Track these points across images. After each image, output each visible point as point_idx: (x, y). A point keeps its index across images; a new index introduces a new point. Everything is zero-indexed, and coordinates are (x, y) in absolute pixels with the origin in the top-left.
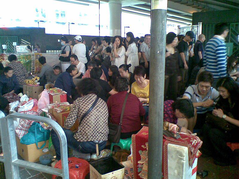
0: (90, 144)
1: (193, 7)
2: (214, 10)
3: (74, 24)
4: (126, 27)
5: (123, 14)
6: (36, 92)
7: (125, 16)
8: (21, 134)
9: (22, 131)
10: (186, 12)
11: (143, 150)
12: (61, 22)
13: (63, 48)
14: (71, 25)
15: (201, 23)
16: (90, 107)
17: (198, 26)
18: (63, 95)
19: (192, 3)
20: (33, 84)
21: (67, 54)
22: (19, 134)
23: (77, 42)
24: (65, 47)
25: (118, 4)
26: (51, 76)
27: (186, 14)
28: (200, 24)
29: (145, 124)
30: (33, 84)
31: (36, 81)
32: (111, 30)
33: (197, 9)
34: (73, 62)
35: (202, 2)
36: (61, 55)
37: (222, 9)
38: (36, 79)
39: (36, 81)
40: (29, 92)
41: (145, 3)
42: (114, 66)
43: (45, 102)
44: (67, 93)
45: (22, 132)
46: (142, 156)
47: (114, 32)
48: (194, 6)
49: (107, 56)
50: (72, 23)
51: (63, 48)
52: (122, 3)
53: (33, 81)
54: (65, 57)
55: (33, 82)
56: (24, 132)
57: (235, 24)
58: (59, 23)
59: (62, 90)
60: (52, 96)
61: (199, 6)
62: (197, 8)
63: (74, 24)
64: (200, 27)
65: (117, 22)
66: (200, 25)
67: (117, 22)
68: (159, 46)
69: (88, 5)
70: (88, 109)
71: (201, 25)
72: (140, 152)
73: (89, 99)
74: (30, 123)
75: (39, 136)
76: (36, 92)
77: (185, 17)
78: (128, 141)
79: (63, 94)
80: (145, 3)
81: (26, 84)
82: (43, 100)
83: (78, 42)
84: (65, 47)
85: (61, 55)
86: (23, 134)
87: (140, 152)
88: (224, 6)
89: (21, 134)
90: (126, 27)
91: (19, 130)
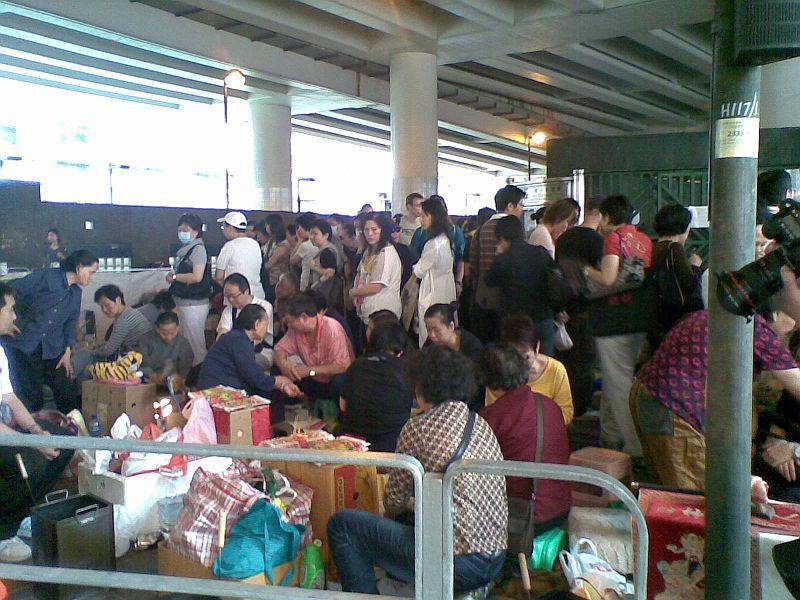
0: (472, 561)
1: (511, 120)
2: (584, 134)
3: (20, 159)
4: (304, 179)
5: (297, 139)
6: (133, 405)
7: (302, 145)
8: (205, 545)
9: (206, 535)
10: (492, 135)
11: (671, 558)
12: (75, 162)
13: (183, 251)
14: (117, 171)
15: (582, 171)
16: (457, 445)
17: (572, 181)
18: (258, 411)
19: (509, 108)
20: (122, 377)
21: (198, 274)
22: (198, 545)
23: (233, 233)
24: (192, 249)
25: (280, 105)
26: (149, 347)
27: (492, 139)
28: (578, 174)
29: (642, 484)
30: (122, 377)
31: (134, 367)
32: (261, 190)
33: (523, 126)
34: (234, 297)
35: (536, 105)
36: (174, 277)
37: (614, 132)
38: (134, 361)
39: (134, 367)
40: (110, 404)
41: (369, 104)
42: (384, 313)
43: (202, 434)
44: (269, 402)
45: (206, 539)
46: (667, 579)
47: (267, 195)
48: (514, 115)
49: (323, 279)
50: (123, 167)
51: (183, 251)
52: (293, 103)
53: (121, 368)
54: (190, 282)
55: (124, 372)
56: (211, 536)
57: (671, 175)
58: (66, 164)
59: (244, 392)
60: (226, 415)
61: (513, 112)
62: (522, 123)
63: (20, 159)
64: (577, 185)
65: (277, 164)
66: (577, 180)
67: (277, 164)
68: (744, 255)
69: (177, 106)
70: (453, 451)
71: (582, 177)
72: (661, 566)
73: (440, 418)
74: (242, 506)
75: (275, 547)
76: (133, 405)
77: (497, 152)
78: (543, 542)
79: (261, 408)
80: (369, 104)
81: (99, 380)
82: (197, 427)
83: (236, 234)
84: (192, 249)
85: (174, 277)
86: (209, 546)
87: (661, 566)
88: (619, 127)
89: (205, 545)
90: (304, 179)
91: (195, 534)
